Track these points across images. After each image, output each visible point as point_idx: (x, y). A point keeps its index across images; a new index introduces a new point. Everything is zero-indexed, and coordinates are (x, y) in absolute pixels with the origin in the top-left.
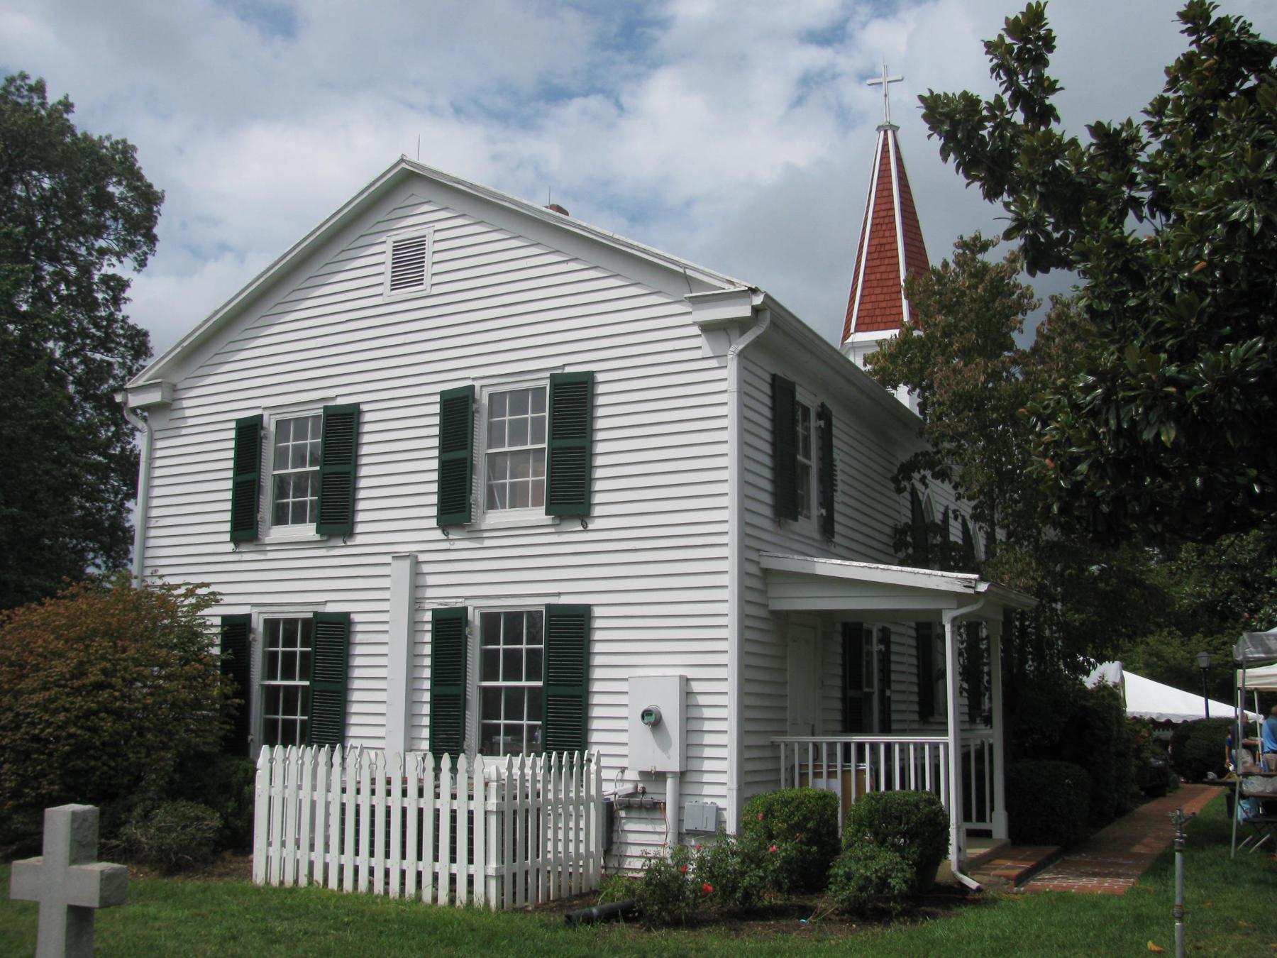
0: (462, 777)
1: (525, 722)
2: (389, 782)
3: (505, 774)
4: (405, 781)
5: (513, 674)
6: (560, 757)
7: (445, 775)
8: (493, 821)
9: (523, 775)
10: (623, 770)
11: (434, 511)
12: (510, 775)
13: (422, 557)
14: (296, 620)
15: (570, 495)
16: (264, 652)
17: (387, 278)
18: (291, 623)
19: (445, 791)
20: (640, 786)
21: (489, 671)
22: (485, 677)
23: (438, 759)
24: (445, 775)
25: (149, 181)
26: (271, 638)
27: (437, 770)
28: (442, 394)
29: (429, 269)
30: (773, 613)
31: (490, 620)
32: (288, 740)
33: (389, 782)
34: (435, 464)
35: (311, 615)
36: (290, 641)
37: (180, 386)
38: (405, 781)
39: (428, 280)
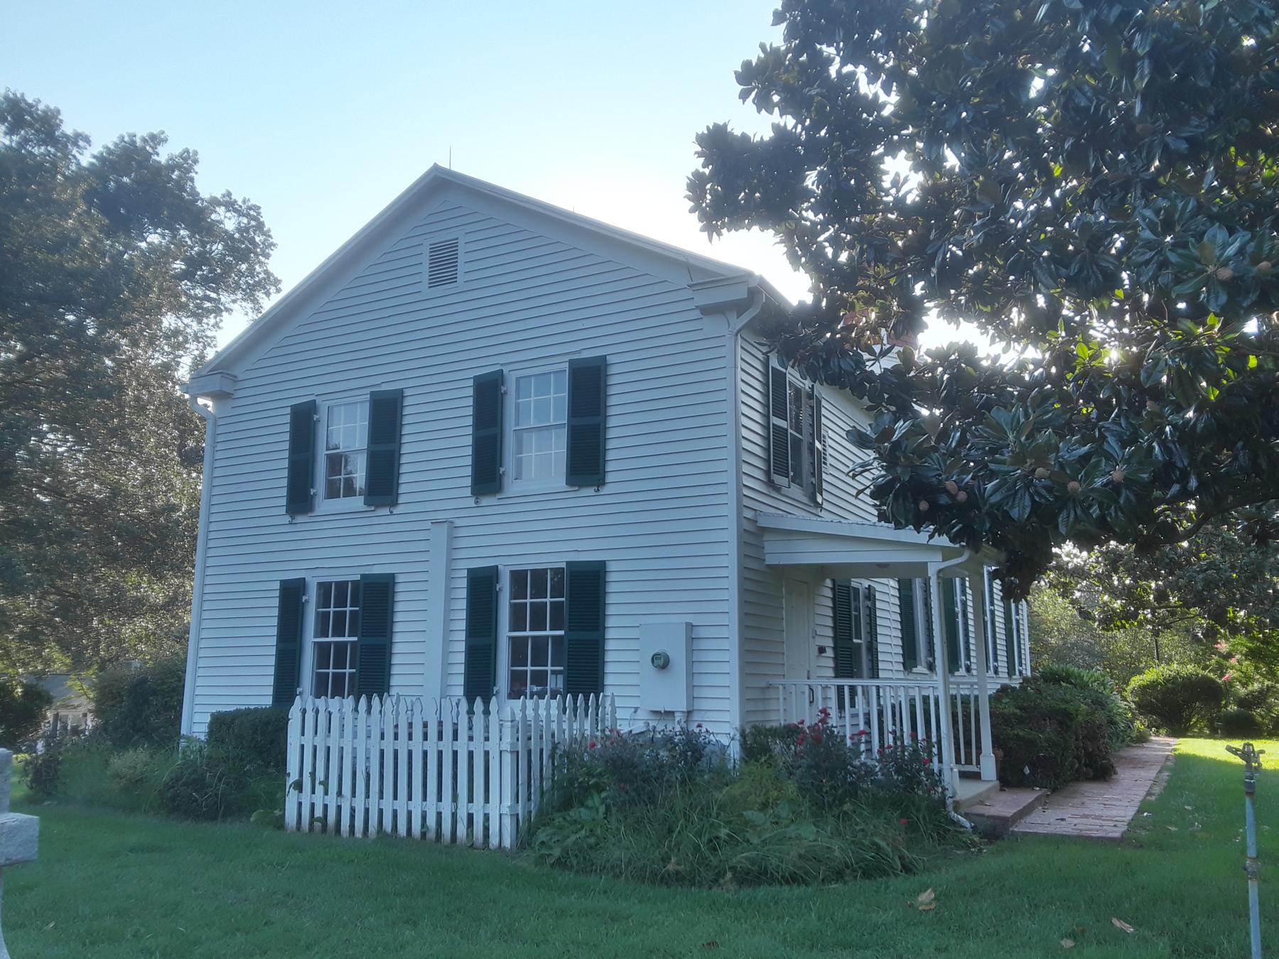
0: (493, 718)
1: (549, 668)
2: (425, 725)
3: (519, 716)
4: (440, 723)
5: (538, 624)
6: (575, 700)
7: (478, 719)
8: (507, 758)
9: (537, 715)
10: (636, 709)
11: (468, 482)
12: (524, 715)
13: (458, 523)
14: (347, 582)
15: (586, 463)
16: (317, 613)
17: (425, 278)
18: (342, 586)
19: (478, 732)
20: (651, 724)
21: (517, 624)
22: (513, 629)
23: (471, 702)
24: (478, 719)
25: (560, 561)
26: (324, 601)
27: (471, 712)
28: (475, 378)
29: (461, 268)
30: (769, 566)
31: (518, 578)
32: (338, 692)
33: (425, 725)
34: (469, 440)
35: (358, 578)
36: (341, 602)
37: (241, 377)
38: (440, 723)
39: (461, 278)
